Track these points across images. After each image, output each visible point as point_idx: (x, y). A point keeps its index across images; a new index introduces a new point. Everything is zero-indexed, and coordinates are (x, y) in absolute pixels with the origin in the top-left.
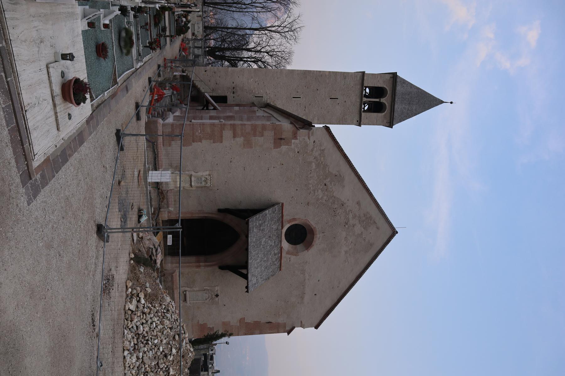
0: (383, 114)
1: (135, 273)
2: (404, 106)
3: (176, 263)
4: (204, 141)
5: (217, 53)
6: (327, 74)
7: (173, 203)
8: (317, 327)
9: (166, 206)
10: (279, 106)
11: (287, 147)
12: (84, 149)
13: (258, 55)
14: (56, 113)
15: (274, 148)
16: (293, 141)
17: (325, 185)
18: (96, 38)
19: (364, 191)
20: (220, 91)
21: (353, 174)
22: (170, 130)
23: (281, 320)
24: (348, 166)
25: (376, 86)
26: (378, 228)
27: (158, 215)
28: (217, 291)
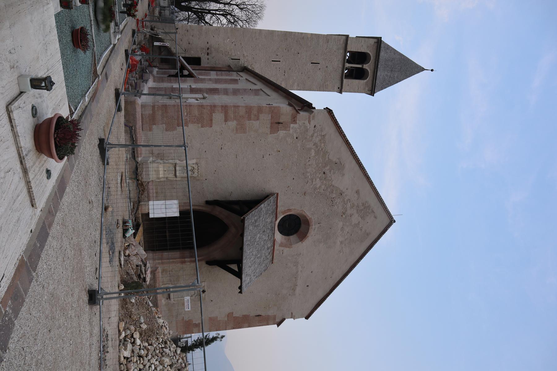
0: (365, 81)
1: (127, 309)
2: (386, 73)
3: (158, 259)
4: (190, 125)
5: (183, 4)
6: (309, 36)
7: (155, 195)
8: (307, 318)
9: (146, 199)
10: (257, 71)
11: (284, 132)
12: (67, 199)
13: (227, 7)
14: (28, 183)
15: (271, 134)
16: (292, 125)
17: (324, 173)
18: (71, 21)
19: (365, 180)
20: (192, 52)
21: (354, 162)
22: (151, 112)
23: (270, 313)
24: (349, 153)
25: (359, 51)
26: (375, 217)
27: (138, 209)
28: (204, 286)
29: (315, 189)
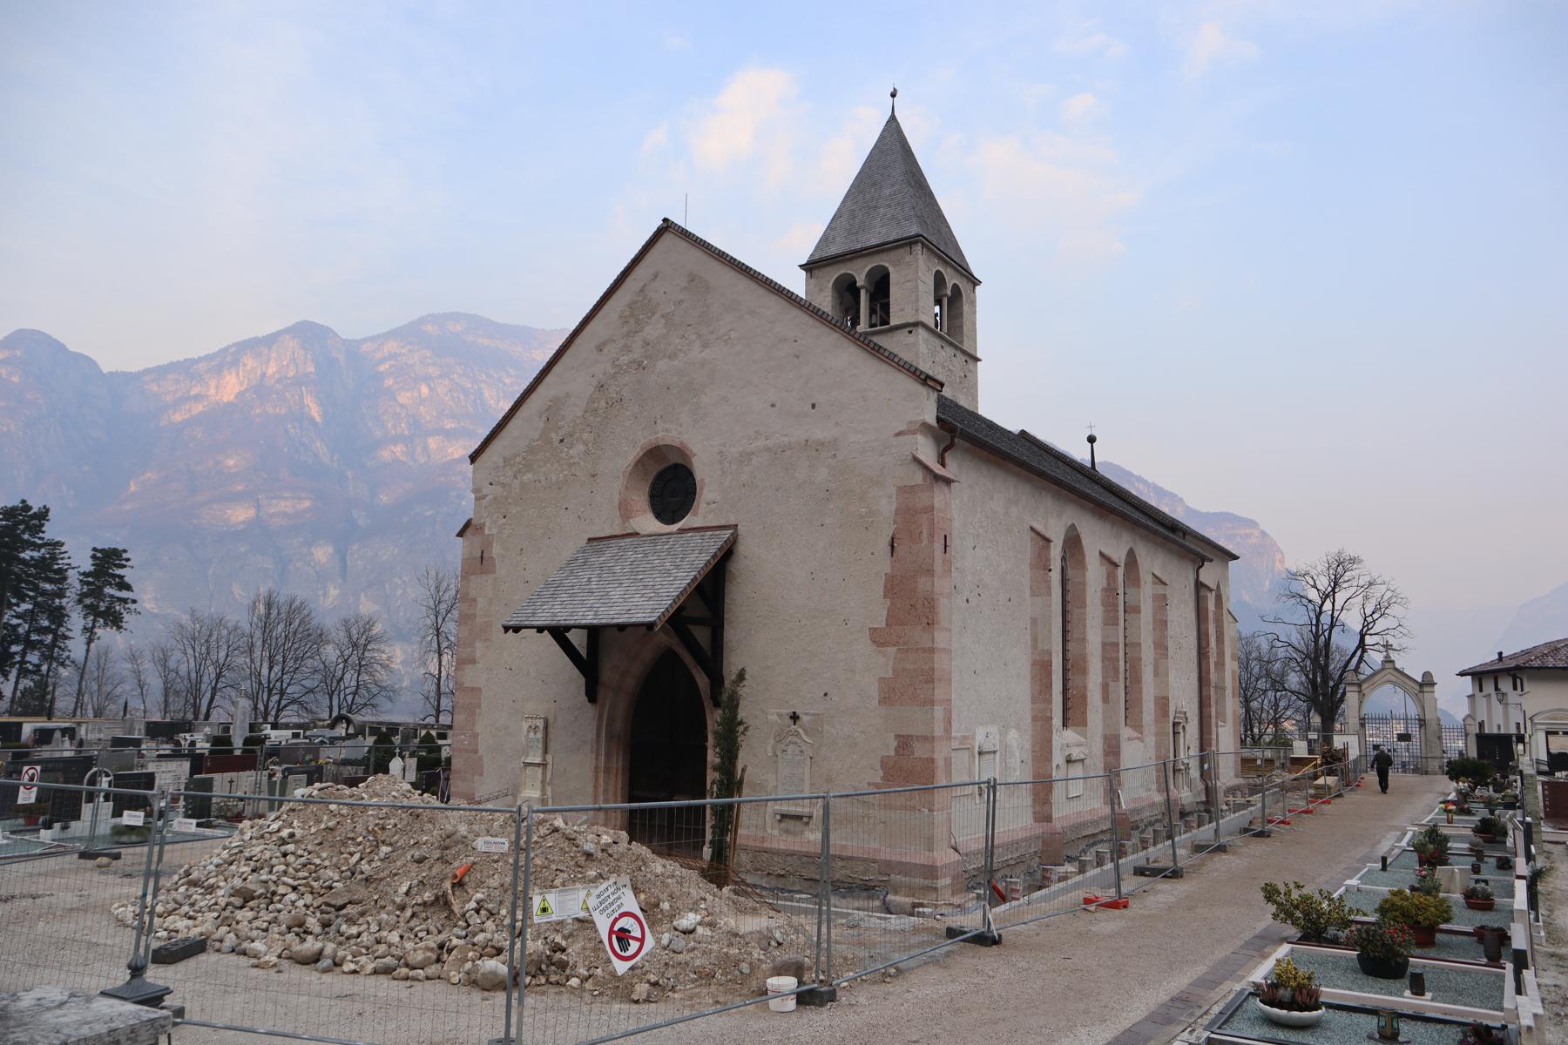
0: (891, 269)
18: (1015, 946)
23: (886, 505)
28: (780, 716)
29: (587, 453)
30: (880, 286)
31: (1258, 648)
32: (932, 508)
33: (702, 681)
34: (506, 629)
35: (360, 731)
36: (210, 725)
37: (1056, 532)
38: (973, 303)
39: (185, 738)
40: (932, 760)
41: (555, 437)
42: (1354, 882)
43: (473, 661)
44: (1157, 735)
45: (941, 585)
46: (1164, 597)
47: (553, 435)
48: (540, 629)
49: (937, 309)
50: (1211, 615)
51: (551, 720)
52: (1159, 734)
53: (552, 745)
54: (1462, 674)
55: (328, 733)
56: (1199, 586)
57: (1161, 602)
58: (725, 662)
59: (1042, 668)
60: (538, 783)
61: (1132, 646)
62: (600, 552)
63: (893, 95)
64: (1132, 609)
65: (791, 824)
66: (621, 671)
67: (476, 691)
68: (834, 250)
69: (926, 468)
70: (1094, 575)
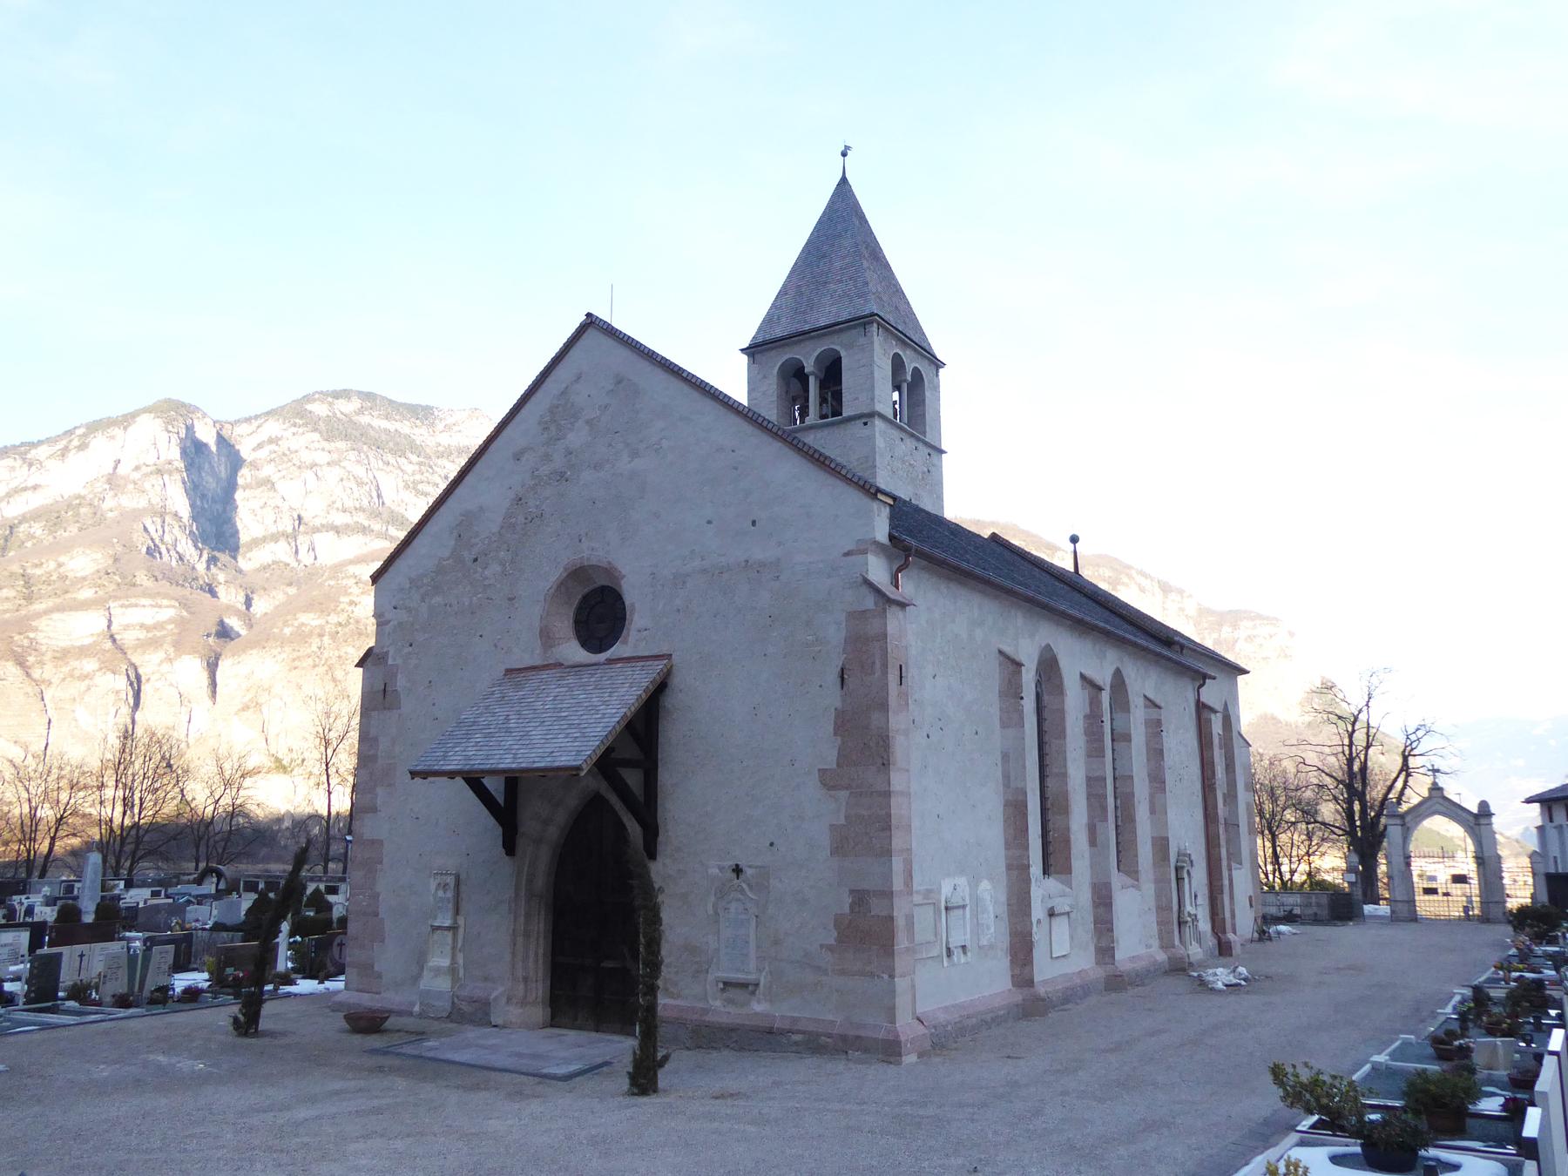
0: (843, 354)
23: (835, 633)
24: (442, 509)
28: (721, 869)
30: (832, 372)
31: (1284, 771)
32: (885, 636)
33: (633, 828)
34: (414, 774)
35: (233, 887)
36: (50, 884)
37: (1028, 653)
38: (936, 388)
39: (19, 902)
40: (891, 918)
41: (467, 556)
42: (1382, 1058)
43: (374, 810)
44: (1157, 881)
45: (897, 721)
46: (1159, 723)
47: (466, 554)
48: (451, 775)
49: (896, 396)
50: (1216, 741)
51: (463, 877)
52: (1160, 881)
53: (464, 905)
54: (1529, 801)
55: (196, 890)
56: (1201, 708)
57: (1155, 729)
58: (660, 810)
59: (1015, 809)
60: (448, 949)
61: (1122, 781)
62: (518, 686)
63: (844, 154)
64: (1121, 737)
65: (732, 993)
66: (545, 823)
67: (376, 844)
68: (779, 332)
69: (877, 591)
70: (1074, 701)
